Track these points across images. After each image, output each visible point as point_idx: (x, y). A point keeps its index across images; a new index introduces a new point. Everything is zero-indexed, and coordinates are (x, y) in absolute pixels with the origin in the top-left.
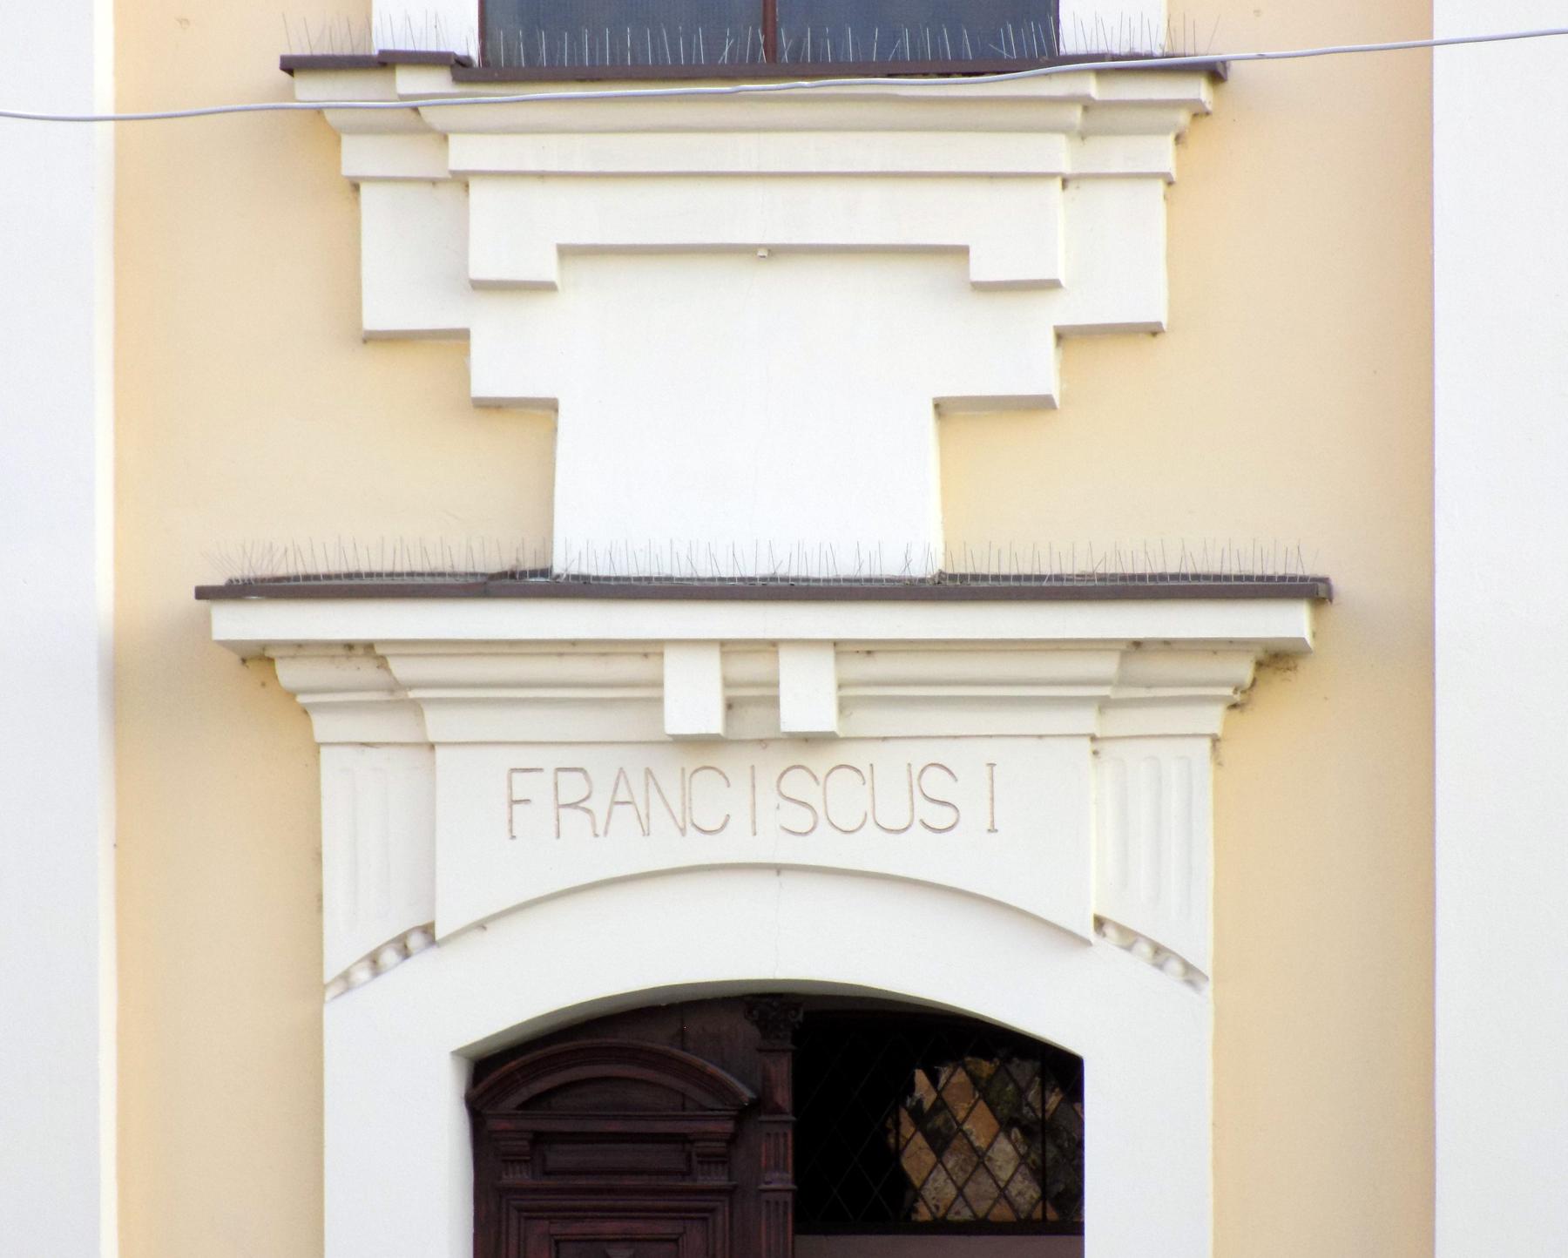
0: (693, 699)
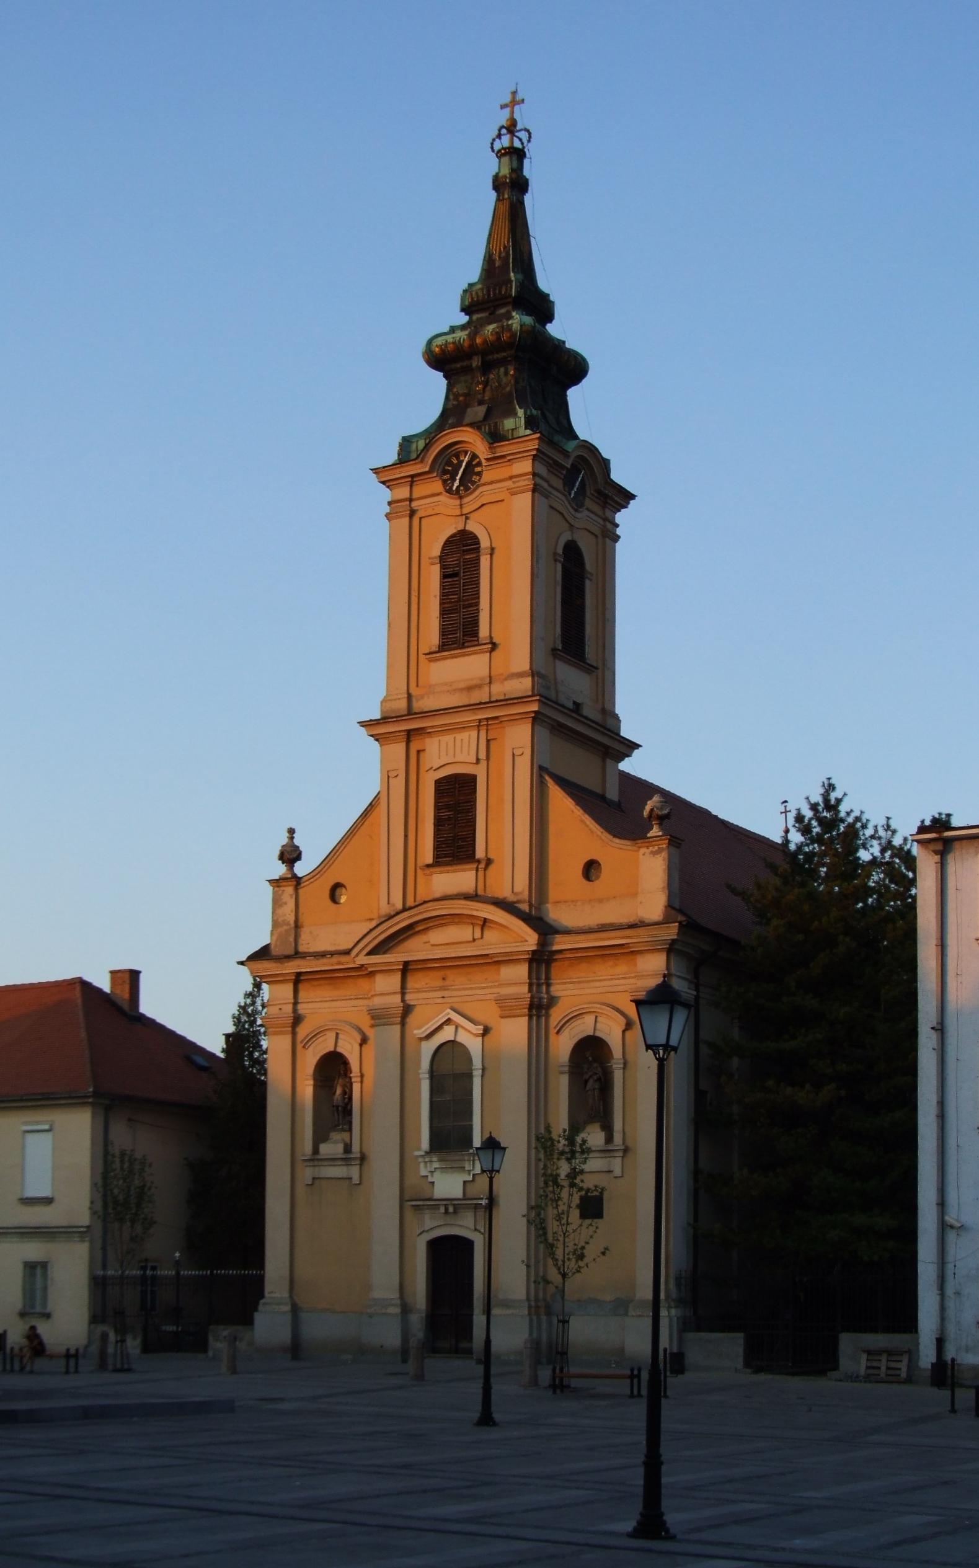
0: (442, 1210)
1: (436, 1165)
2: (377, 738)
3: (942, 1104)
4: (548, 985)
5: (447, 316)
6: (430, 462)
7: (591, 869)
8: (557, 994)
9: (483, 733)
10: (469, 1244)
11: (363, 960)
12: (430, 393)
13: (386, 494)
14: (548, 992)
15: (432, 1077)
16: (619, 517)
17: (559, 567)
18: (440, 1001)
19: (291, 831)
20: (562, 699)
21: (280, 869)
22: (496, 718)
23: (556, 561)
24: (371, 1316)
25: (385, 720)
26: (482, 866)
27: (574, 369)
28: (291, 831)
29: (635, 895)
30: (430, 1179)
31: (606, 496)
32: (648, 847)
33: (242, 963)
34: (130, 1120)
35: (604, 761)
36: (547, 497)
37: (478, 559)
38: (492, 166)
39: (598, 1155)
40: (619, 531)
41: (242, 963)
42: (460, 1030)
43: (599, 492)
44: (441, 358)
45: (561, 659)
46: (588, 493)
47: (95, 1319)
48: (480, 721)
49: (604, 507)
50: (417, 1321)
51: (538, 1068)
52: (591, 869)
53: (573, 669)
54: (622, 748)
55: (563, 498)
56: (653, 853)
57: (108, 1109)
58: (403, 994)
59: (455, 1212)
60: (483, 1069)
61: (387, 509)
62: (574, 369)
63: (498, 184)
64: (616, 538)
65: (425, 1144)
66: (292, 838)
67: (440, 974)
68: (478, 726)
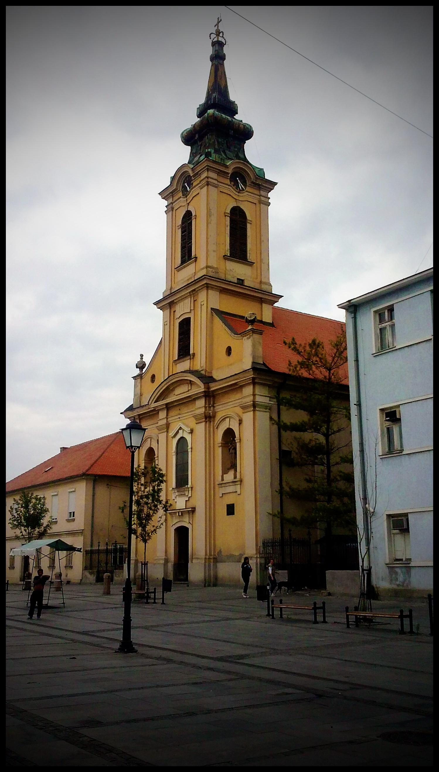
1: (177, 494)
2: (161, 308)
3: (362, 444)
4: (214, 407)
5: (192, 120)
6: (182, 184)
7: (229, 351)
8: (217, 411)
9: (192, 298)
10: (188, 529)
11: (153, 405)
12: (183, 154)
13: (165, 203)
14: (214, 410)
15: (177, 454)
16: (270, 195)
17: (228, 219)
18: (178, 419)
19: (142, 356)
20: (229, 278)
21: (137, 372)
22: (194, 290)
23: (225, 216)
24: (155, 564)
25: (164, 299)
26: (192, 357)
27: (246, 133)
28: (142, 356)
29: (241, 360)
30: (175, 500)
31: (259, 185)
32: (246, 336)
33: (121, 413)
34: (107, 485)
35: (262, 305)
36: (216, 187)
37: (191, 222)
38: (210, 51)
39: (231, 484)
40: (270, 201)
41: (121, 413)
42: (185, 432)
43: (253, 182)
44: (189, 138)
45: (228, 260)
46: (248, 184)
47: (85, 568)
48: (190, 292)
49: (260, 190)
50: (170, 566)
51: (210, 447)
52: (229, 351)
53: (242, 265)
54: (272, 299)
55: (231, 188)
56: (248, 338)
57: (95, 481)
58: (167, 419)
59: (182, 515)
60: (191, 448)
61: (166, 209)
62: (246, 133)
63: (212, 59)
64: (269, 204)
65: (174, 486)
66: (142, 358)
67: (178, 408)
68: (190, 295)
